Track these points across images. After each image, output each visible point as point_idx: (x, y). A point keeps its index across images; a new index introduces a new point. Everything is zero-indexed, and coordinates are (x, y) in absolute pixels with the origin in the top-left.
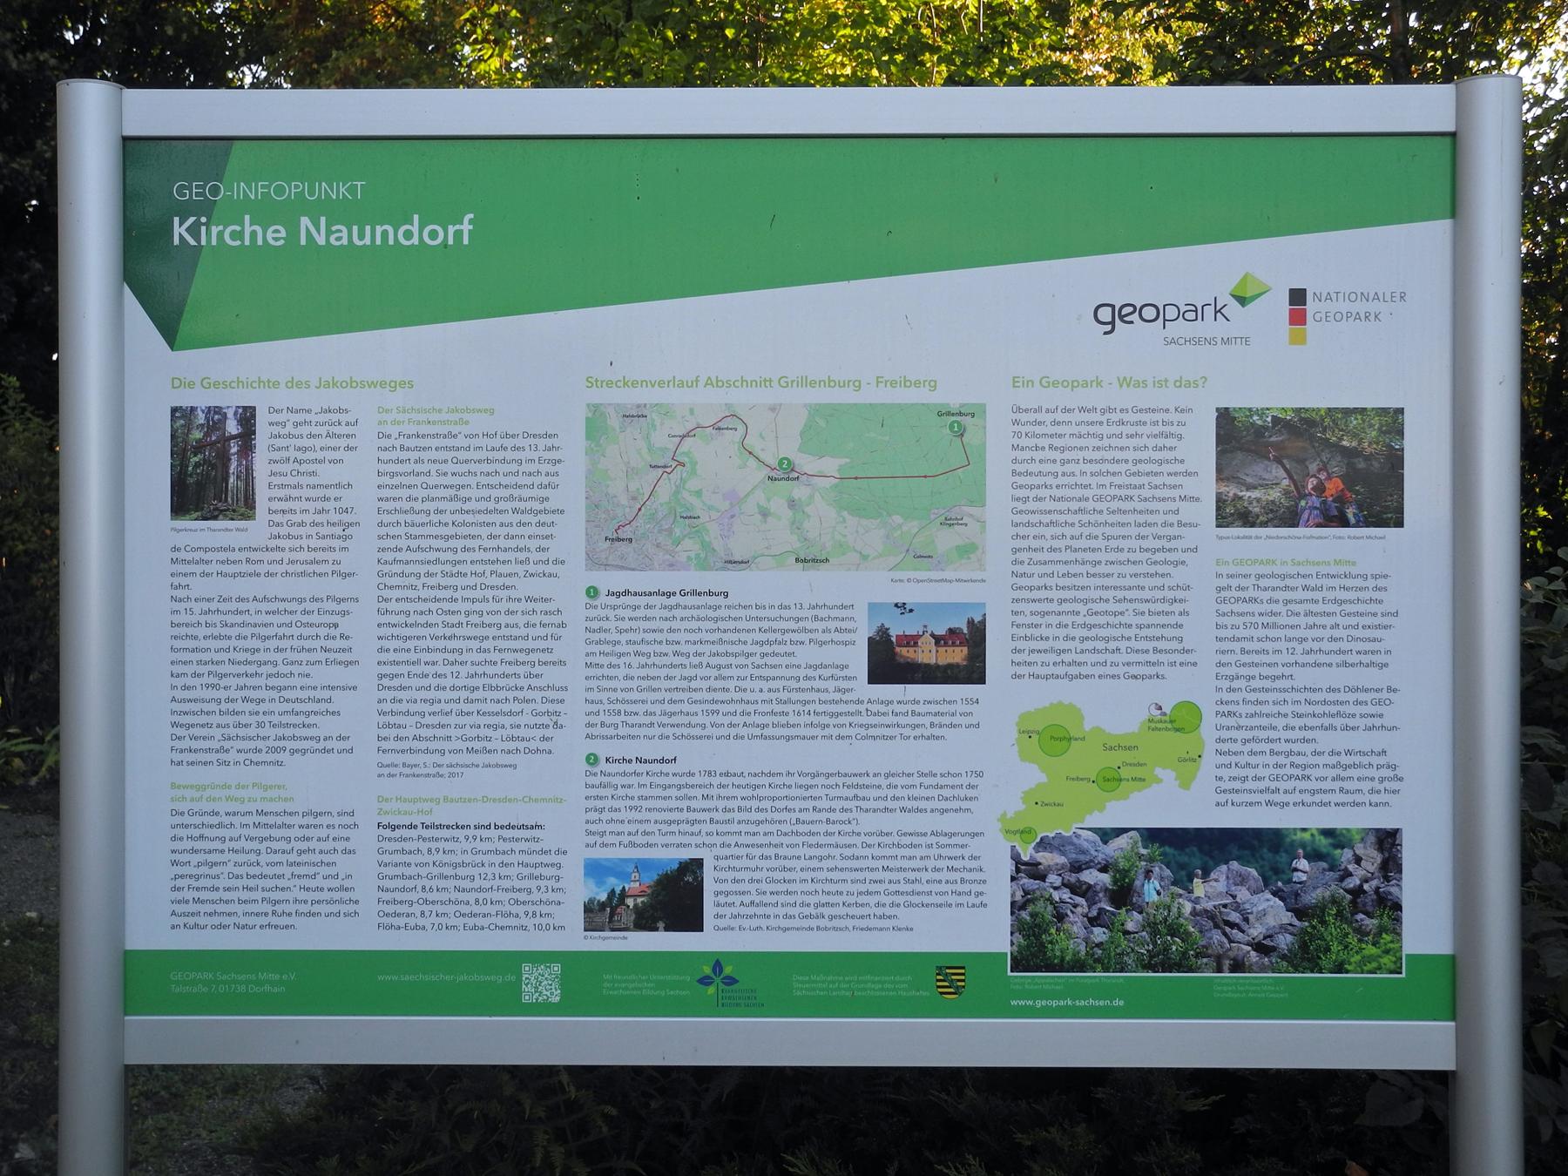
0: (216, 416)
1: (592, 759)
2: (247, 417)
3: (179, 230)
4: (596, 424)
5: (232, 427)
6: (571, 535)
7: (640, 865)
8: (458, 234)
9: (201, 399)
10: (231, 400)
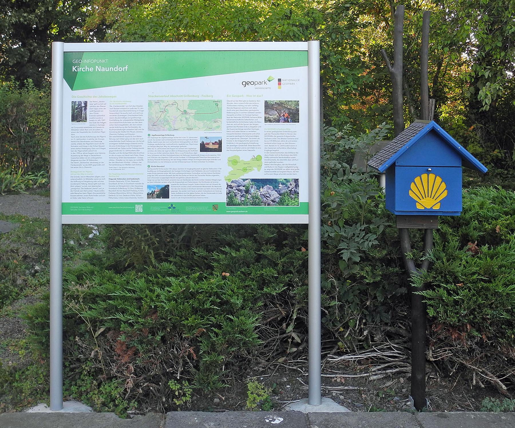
0: (80, 103)
1: (149, 166)
2: (86, 103)
3: (74, 69)
4: (150, 104)
5: (83, 105)
6: (145, 125)
7: (158, 186)
8: (125, 69)
9: (77, 100)
10: (83, 100)
